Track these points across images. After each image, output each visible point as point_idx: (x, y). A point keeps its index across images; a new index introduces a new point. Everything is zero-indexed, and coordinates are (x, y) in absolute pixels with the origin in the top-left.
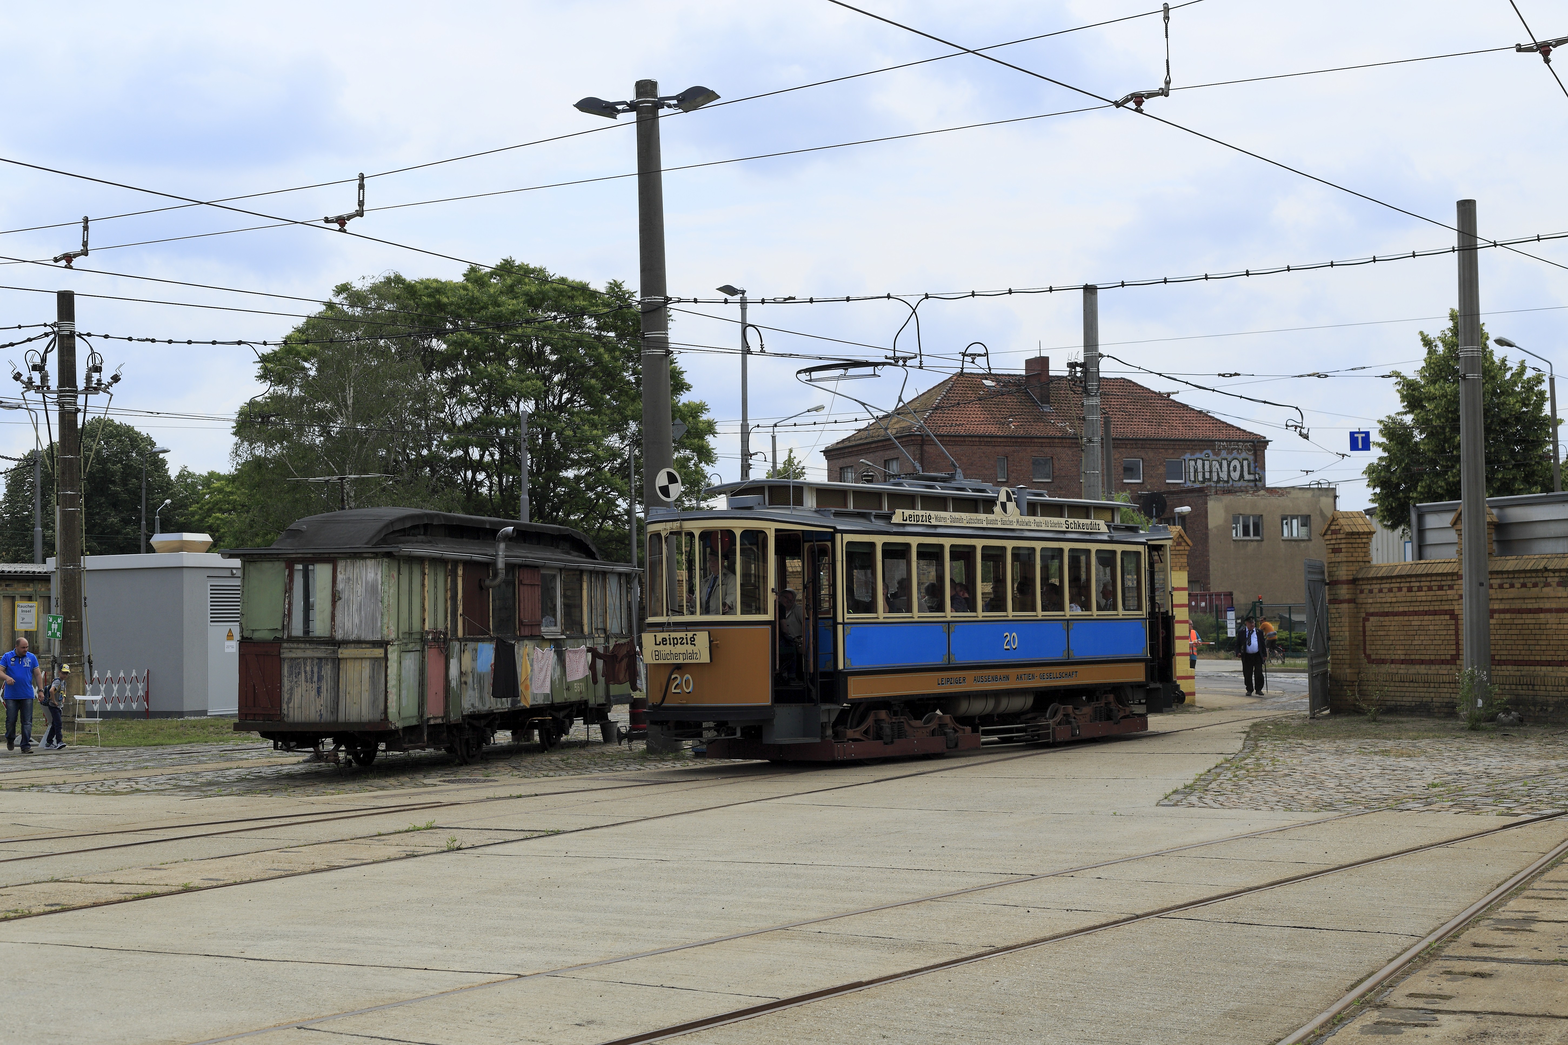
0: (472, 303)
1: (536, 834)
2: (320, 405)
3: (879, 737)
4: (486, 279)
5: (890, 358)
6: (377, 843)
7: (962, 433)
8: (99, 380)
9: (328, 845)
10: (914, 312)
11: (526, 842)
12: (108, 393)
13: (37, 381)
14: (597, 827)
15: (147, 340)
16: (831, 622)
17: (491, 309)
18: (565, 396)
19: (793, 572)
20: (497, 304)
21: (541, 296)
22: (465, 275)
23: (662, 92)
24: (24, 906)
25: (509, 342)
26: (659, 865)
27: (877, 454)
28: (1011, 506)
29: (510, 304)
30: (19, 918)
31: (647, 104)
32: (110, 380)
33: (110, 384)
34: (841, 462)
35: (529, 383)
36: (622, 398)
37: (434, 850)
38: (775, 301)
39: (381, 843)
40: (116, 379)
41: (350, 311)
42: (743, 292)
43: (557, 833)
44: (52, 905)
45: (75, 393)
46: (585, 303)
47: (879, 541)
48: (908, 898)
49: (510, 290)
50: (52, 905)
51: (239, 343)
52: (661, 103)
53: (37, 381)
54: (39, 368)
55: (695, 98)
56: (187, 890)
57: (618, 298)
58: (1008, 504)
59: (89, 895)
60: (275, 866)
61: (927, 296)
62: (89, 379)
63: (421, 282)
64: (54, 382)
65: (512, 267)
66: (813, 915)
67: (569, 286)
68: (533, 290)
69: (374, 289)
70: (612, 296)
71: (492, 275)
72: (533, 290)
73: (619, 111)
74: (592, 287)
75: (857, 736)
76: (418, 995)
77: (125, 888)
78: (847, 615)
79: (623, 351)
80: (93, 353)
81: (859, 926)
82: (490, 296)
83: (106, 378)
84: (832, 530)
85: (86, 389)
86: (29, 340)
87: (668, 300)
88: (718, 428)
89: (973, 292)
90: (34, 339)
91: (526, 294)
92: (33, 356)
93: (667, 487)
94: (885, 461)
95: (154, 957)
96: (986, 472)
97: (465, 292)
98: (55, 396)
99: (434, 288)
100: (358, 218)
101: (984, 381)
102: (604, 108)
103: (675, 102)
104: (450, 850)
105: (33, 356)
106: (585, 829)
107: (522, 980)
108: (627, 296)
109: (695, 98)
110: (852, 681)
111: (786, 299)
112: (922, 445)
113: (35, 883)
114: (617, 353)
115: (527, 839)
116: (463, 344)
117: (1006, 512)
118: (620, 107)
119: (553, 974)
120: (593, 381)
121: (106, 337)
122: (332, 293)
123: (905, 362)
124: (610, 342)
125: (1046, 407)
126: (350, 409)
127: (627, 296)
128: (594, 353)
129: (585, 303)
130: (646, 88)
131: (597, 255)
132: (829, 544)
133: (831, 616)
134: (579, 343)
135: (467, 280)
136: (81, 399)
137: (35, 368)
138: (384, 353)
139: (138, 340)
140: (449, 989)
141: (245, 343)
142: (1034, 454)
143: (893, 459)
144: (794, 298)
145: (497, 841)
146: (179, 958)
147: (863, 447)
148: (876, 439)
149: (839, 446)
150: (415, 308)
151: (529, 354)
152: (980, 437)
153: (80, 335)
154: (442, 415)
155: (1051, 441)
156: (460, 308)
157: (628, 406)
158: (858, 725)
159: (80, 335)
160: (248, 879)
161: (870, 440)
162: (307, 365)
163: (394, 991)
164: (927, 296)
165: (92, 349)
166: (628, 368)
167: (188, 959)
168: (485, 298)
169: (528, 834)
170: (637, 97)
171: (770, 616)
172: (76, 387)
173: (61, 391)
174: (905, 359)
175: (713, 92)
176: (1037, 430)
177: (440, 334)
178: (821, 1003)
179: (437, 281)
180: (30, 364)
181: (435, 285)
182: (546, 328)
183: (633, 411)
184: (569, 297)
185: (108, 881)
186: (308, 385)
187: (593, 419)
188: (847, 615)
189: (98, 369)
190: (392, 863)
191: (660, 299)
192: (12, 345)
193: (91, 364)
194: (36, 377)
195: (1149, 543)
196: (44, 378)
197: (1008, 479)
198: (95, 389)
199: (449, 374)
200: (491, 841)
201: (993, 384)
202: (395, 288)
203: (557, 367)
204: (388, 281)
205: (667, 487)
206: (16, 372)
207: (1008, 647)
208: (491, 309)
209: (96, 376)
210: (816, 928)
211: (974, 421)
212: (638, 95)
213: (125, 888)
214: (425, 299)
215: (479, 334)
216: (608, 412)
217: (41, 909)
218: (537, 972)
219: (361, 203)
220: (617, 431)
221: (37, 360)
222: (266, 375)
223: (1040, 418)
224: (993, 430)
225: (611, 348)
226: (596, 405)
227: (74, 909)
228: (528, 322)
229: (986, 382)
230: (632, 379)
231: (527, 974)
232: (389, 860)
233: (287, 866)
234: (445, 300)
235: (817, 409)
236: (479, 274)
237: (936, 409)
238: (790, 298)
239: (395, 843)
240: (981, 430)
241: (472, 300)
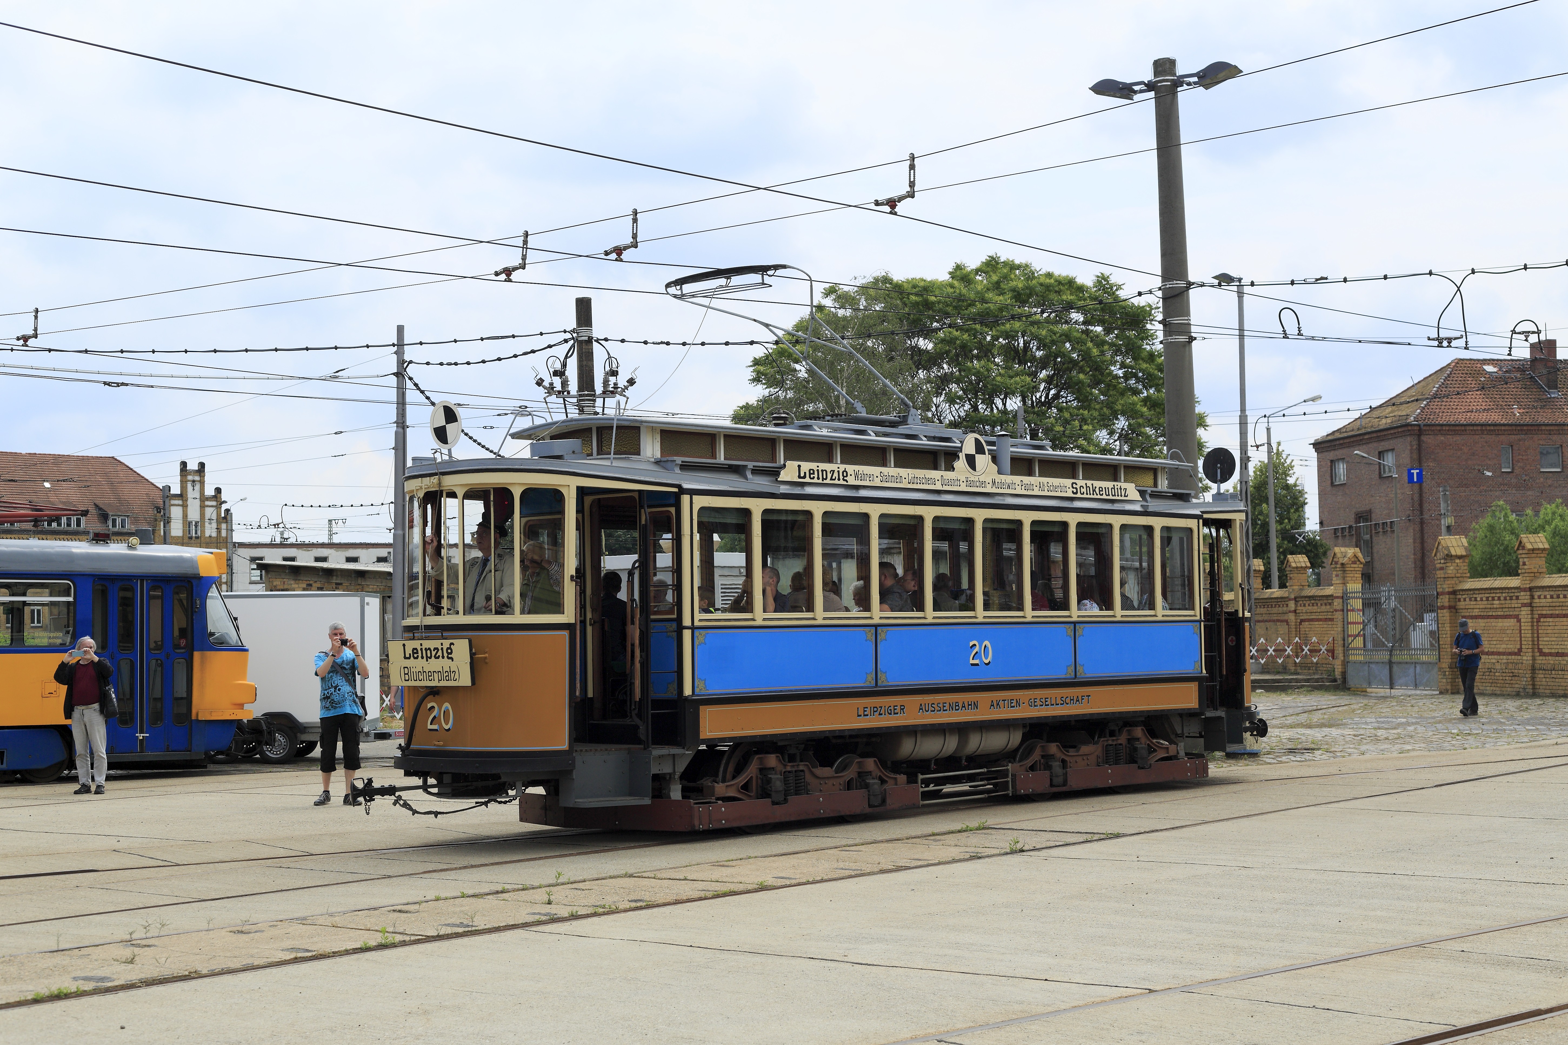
0: (959, 300)
1: (1096, 837)
2: (811, 407)
4: (972, 276)
5: (1433, 339)
6: (934, 843)
7: (1463, 422)
8: (615, 384)
9: (886, 845)
10: (1459, 290)
11: (1089, 845)
12: (625, 396)
13: (558, 386)
14: (1157, 831)
15: (662, 343)
17: (978, 305)
18: (1053, 392)
19: (1297, 568)
20: (984, 301)
21: (1028, 291)
22: (950, 273)
23: (1180, 70)
24: (609, 901)
25: (995, 338)
26: (1244, 872)
27: (1370, 445)
28: (983, 461)
29: (997, 299)
30: (608, 913)
31: (1165, 84)
32: (626, 384)
33: (626, 388)
34: (1332, 455)
35: (1018, 379)
36: (1111, 393)
37: (997, 851)
38: (1305, 282)
39: (938, 843)
40: (631, 382)
41: (841, 313)
42: (1240, 280)
43: (1117, 836)
44: (635, 901)
45: (593, 397)
46: (1072, 297)
48: (1543, 915)
49: (997, 287)
50: (635, 901)
51: (752, 343)
52: (1179, 82)
53: (558, 386)
54: (560, 374)
55: (1216, 74)
56: (763, 888)
57: (1105, 290)
58: (978, 457)
59: (667, 891)
60: (841, 865)
61: (1473, 272)
62: (606, 383)
63: (908, 282)
64: (573, 386)
65: (997, 263)
66: (1445, 932)
67: (1056, 281)
68: (1020, 285)
69: (864, 289)
70: (1099, 290)
71: (977, 271)
72: (1020, 285)
73: (1135, 92)
74: (1080, 281)
75: (732, 793)
76: (1050, 1009)
77: (701, 885)
79: (1112, 345)
80: (610, 357)
81: (1502, 945)
82: (978, 293)
83: (622, 381)
84: (676, 490)
85: (604, 392)
86: (550, 346)
87: (1190, 285)
88: (1209, 421)
89: (1525, 265)
90: (554, 345)
91: (1013, 290)
92: (554, 362)
94: (1380, 453)
95: (758, 959)
96: (1489, 462)
97: (952, 290)
98: (575, 400)
99: (921, 287)
100: (909, 199)
101: (1486, 367)
102: (1121, 89)
103: (1195, 79)
104: (1013, 852)
105: (554, 362)
106: (1145, 832)
107: (1152, 996)
108: (1115, 288)
109: (1216, 74)
110: (707, 714)
111: (1317, 280)
112: (1419, 436)
113: (611, 877)
114: (1106, 347)
115: (1087, 842)
116: (951, 341)
118: (1136, 88)
119: (1187, 989)
120: (1082, 376)
121: (623, 341)
122: (821, 295)
123: (1449, 343)
124: (1097, 336)
125: (1554, 393)
126: (843, 409)
127: (1115, 288)
128: (1083, 348)
129: (1072, 297)
130: (1164, 66)
131: (1106, 244)
132: (673, 510)
133: (675, 616)
134: (1067, 336)
135: (953, 278)
136: (599, 402)
137: (556, 373)
138: (871, 354)
139: (654, 343)
140: (1081, 1003)
141: (757, 343)
142: (1541, 442)
143: (1388, 451)
144: (1326, 278)
145: (1058, 844)
146: (784, 960)
147: (1355, 439)
148: (1369, 430)
149: (1330, 438)
150: (906, 308)
151: (1016, 350)
152: (1482, 425)
153: (597, 341)
154: (930, 415)
155: (1560, 428)
156: (947, 305)
157: (1117, 401)
159: (597, 341)
160: (819, 878)
161: (1363, 431)
162: (797, 367)
163: (1022, 1003)
164: (1473, 272)
165: (609, 354)
166: (1116, 361)
167: (794, 961)
168: (972, 296)
169: (1089, 837)
170: (1155, 76)
171: (568, 616)
172: (594, 391)
173: (580, 396)
174: (1450, 340)
175: (1236, 67)
176: (1544, 417)
177: (927, 333)
178: (1504, 1033)
179: (922, 280)
180: (552, 370)
181: (922, 284)
182: (1033, 323)
183: (1123, 406)
184: (1056, 292)
185: (682, 877)
186: (800, 386)
187: (1082, 414)
188: (698, 616)
189: (614, 373)
190: (959, 864)
191: (1182, 284)
192: (533, 352)
193: (608, 369)
194: (557, 382)
195: (1205, 516)
196: (564, 384)
197: (1513, 469)
198: (612, 392)
199: (935, 372)
200: (1053, 844)
201: (1495, 370)
202: (884, 288)
203: (1043, 364)
204: (877, 280)
206: (538, 377)
208: (978, 305)
209: (612, 380)
210: (1457, 946)
211: (1474, 408)
212: (1156, 74)
213: (701, 885)
214: (913, 298)
215: (967, 331)
216: (1097, 407)
217: (628, 905)
218: (1167, 987)
219: (912, 184)
220: (1106, 426)
221: (558, 366)
222: (759, 377)
223: (1547, 403)
224: (1495, 417)
225: (1100, 343)
226: (1085, 401)
227: (658, 906)
228: (1013, 317)
229: (1486, 367)
230: (1120, 373)
231: (1158, 988)
232: (954, 861)
233: (853, 866)
234: (933, 299)
235: (1313, 400)
236: (964, 272)
237: (1435, 396)
238: (1322, 278)
239: (953, 843)
240: (1483, 418)
241: (960, 298)
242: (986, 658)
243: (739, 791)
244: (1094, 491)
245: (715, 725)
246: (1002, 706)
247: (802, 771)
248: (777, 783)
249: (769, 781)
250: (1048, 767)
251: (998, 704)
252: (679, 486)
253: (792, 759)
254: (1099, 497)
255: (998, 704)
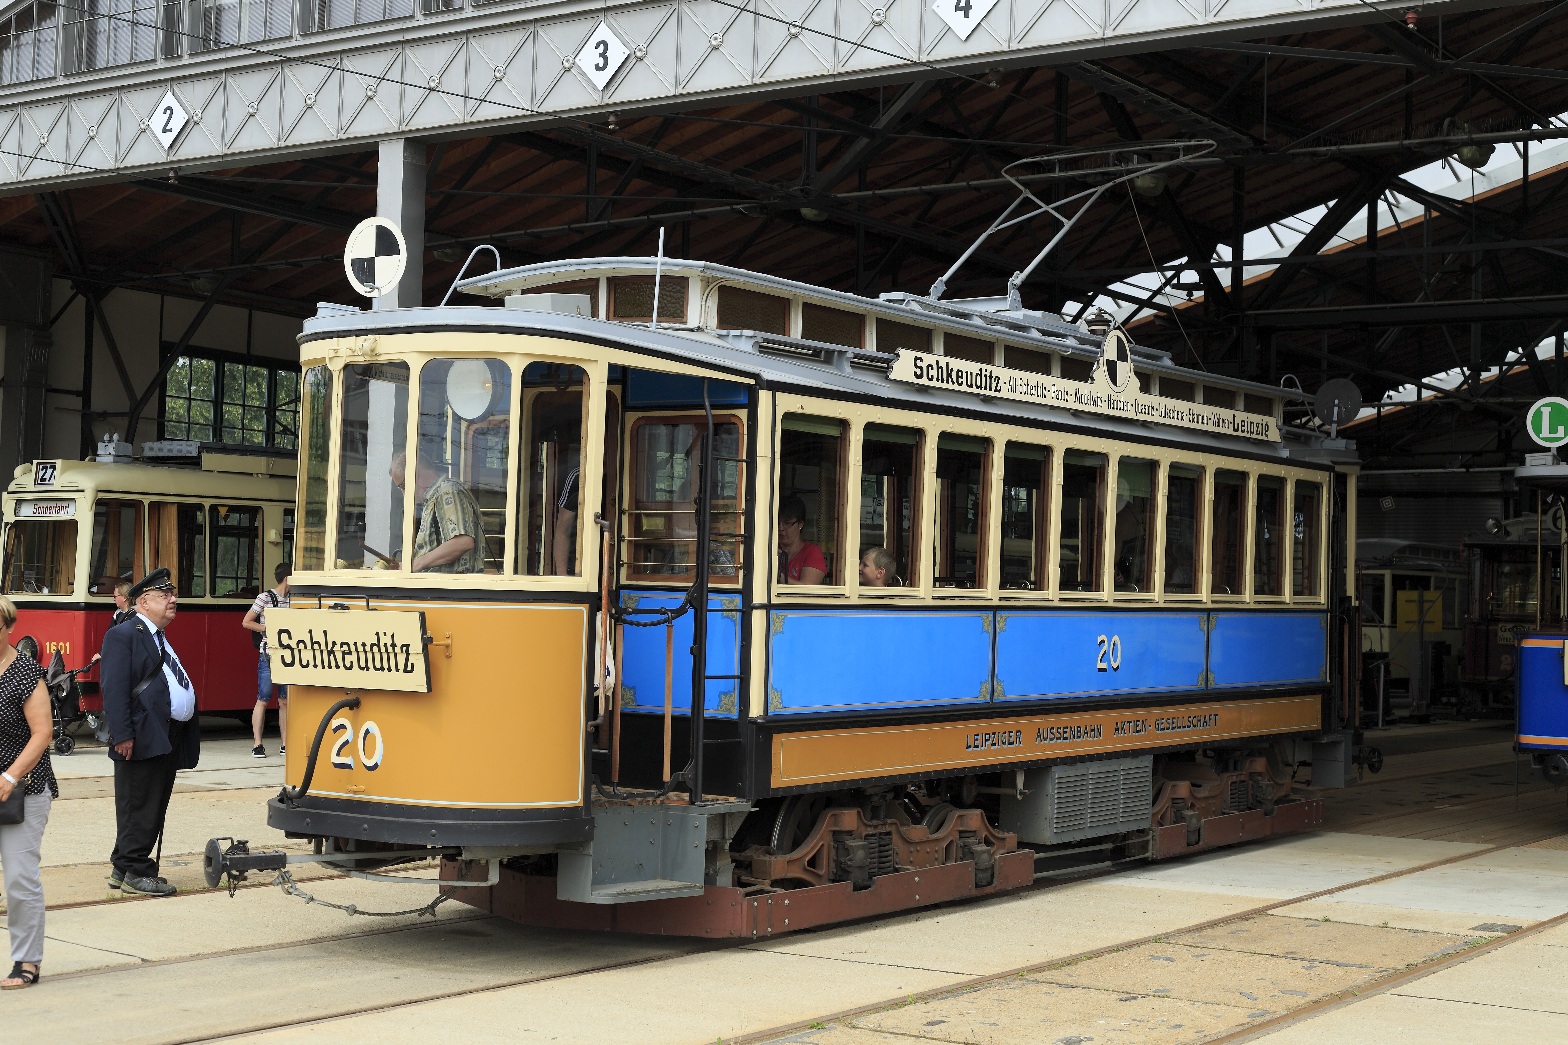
3: (840, 875)
16: (737, 601)
28: (1125, 370)
47: (1060, 443)
58: (1121, 365)
75: (796, 873)
78: (776, 588)
84: (752, 382)
93: (371, 261)
110: (783, 746)
117: (1114, 382)
132: (743, 414)
133: (740, 586)
158: (796, 844)
171: (586, 580)
188: (776, 588)
205: (371, 261)
207: (1103, 666)
242: (1115, 661)
243: (805, 870)
244: (949, 375)
245: (794, 765)
246: (1127, 730)
247: (889, 833)
248: (858, 851)
249: (847, 851)
250: (1179, 818)
251: (1123, 728)
252: (755, 376)
253: (875, 815)
254: (956, 387)
255: (1123, 728)
